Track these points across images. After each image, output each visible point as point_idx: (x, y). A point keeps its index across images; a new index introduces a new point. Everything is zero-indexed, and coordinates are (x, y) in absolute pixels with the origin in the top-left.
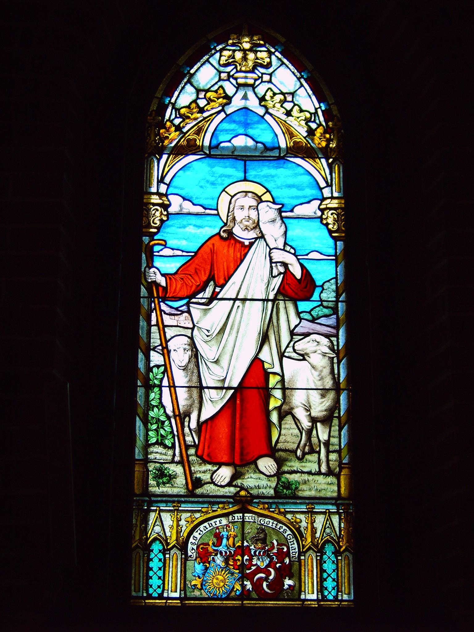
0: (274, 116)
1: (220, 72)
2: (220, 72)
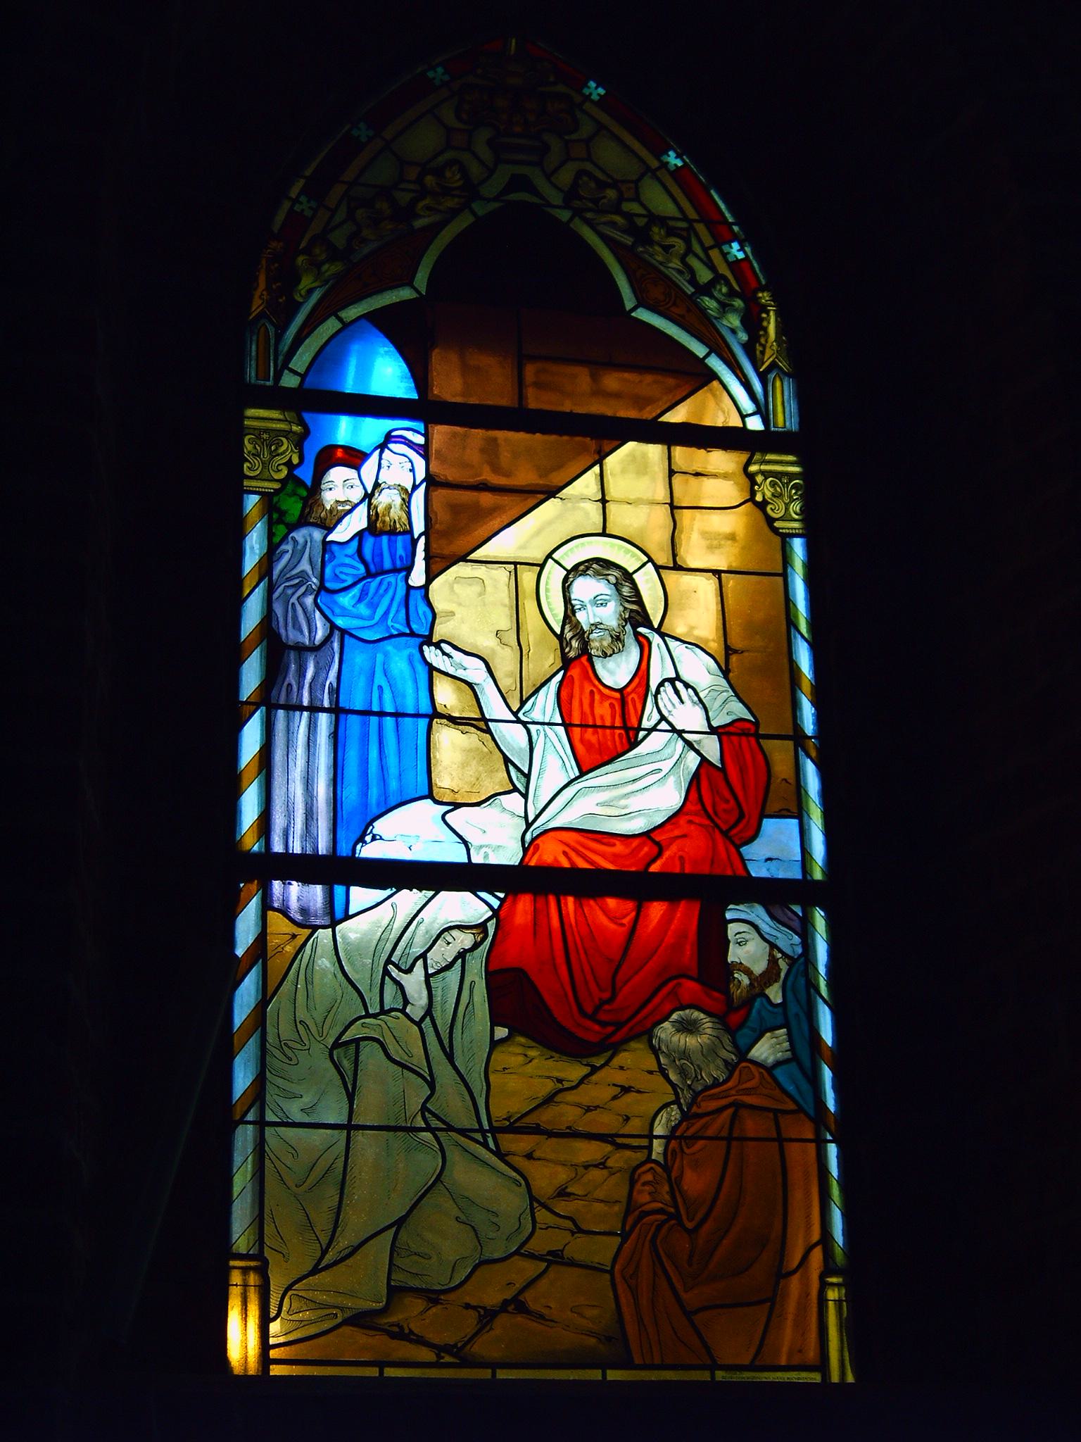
0: (679, 232)
1: (589, 158)
2: (589, 158)
